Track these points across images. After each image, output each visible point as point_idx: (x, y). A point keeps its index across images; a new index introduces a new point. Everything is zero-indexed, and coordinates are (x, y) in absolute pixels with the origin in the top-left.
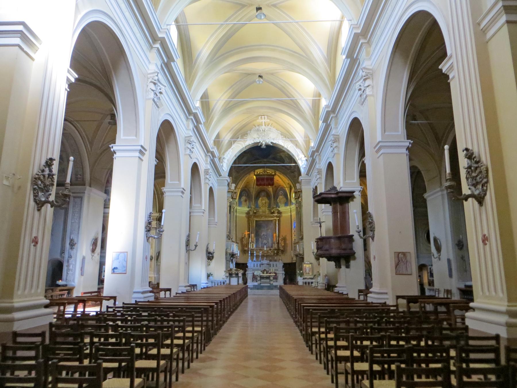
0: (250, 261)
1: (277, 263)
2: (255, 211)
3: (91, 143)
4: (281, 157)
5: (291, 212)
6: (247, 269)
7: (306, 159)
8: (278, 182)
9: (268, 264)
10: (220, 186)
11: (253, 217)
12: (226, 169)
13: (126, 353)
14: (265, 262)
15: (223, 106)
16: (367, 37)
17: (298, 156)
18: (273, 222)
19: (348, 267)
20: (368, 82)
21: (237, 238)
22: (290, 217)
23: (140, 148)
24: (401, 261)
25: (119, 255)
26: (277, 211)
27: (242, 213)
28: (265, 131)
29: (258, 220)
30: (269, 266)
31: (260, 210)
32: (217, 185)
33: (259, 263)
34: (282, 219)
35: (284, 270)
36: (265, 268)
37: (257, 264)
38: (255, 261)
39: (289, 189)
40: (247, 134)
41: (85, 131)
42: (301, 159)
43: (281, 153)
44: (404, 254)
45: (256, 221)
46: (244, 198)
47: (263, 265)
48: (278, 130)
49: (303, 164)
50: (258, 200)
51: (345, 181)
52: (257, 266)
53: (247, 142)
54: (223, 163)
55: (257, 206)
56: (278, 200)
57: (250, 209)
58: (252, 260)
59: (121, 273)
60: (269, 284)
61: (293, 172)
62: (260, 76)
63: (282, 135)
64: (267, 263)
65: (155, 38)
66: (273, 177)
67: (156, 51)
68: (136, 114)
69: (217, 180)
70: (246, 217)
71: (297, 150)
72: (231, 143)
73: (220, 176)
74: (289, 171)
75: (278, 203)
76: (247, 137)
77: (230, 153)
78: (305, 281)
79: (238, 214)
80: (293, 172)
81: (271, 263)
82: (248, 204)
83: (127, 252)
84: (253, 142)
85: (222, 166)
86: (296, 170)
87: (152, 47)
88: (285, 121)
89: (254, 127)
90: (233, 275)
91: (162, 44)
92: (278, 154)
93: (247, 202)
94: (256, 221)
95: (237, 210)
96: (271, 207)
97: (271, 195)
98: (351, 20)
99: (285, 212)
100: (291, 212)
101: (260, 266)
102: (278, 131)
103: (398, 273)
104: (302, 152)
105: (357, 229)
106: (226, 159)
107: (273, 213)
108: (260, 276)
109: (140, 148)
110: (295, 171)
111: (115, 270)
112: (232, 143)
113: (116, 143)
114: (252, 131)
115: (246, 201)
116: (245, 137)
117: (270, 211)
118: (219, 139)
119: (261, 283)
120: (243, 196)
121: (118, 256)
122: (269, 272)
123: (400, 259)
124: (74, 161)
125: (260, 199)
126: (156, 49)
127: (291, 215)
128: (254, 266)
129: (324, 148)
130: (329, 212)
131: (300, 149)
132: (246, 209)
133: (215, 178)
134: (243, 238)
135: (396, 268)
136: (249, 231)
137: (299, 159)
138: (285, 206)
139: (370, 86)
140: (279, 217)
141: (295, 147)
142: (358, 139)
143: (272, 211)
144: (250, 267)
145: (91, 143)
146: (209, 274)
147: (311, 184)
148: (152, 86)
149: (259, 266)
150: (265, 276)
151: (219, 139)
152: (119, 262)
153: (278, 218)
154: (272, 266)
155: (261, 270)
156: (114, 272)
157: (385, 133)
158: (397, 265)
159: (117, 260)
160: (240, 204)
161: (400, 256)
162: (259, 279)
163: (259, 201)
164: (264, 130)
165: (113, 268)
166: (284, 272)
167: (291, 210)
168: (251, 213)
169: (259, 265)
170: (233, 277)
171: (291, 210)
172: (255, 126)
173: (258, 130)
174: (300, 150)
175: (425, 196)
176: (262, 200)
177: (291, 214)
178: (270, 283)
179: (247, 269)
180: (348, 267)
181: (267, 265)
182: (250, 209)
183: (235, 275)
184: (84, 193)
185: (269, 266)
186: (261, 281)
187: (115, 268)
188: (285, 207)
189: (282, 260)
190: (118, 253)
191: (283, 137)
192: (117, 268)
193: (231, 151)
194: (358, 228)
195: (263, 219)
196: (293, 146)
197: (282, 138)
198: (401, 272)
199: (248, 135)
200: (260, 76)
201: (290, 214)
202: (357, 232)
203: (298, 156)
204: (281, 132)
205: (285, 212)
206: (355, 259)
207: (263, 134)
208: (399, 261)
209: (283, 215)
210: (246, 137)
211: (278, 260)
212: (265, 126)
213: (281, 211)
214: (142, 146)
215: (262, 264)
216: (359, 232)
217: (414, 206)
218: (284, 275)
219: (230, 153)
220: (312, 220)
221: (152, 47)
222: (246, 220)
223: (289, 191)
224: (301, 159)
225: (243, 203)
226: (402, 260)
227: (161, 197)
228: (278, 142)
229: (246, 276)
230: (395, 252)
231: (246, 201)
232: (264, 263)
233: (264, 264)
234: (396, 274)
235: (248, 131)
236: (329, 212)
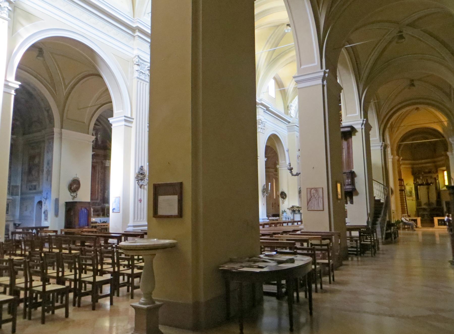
10: (290, 132)
12: (295, 115)
15: (266, 60)
19: (352, 202)
23: (124, 118)
24: (313, 197)
25: (116, 199)
44: (316, 190)
51: (346, 116)
54: (291, 110)
59: (117, 212)
65: (133, 29)
67: (138, 38)
68: (121, 93)
87: (134, 37)
90: (296, 212)
91: (140, 30)
103: (310, 209)
106: (293, 106)
109: (124, 118)
111: (114, 210)
113: (114, 116)
118: (284, 88)
121: (115, 200)
123: (312, 195)
126: (137, 36)
130: (373, 146)
142: (351, 71)
146: (283, 211)
148: (136, 68)
151: (281, 91)
156: (113, 211)
157: (301, 67)
165: (113, 209)
170: (296, 213)
180: (352, 202)
190: (115, 198)
198: (312, 209)
206: (357, 194)
208: (311, 197)
214: (125, 116)
221: (134, 37)
226: (314, 196)
236: (373, 146)
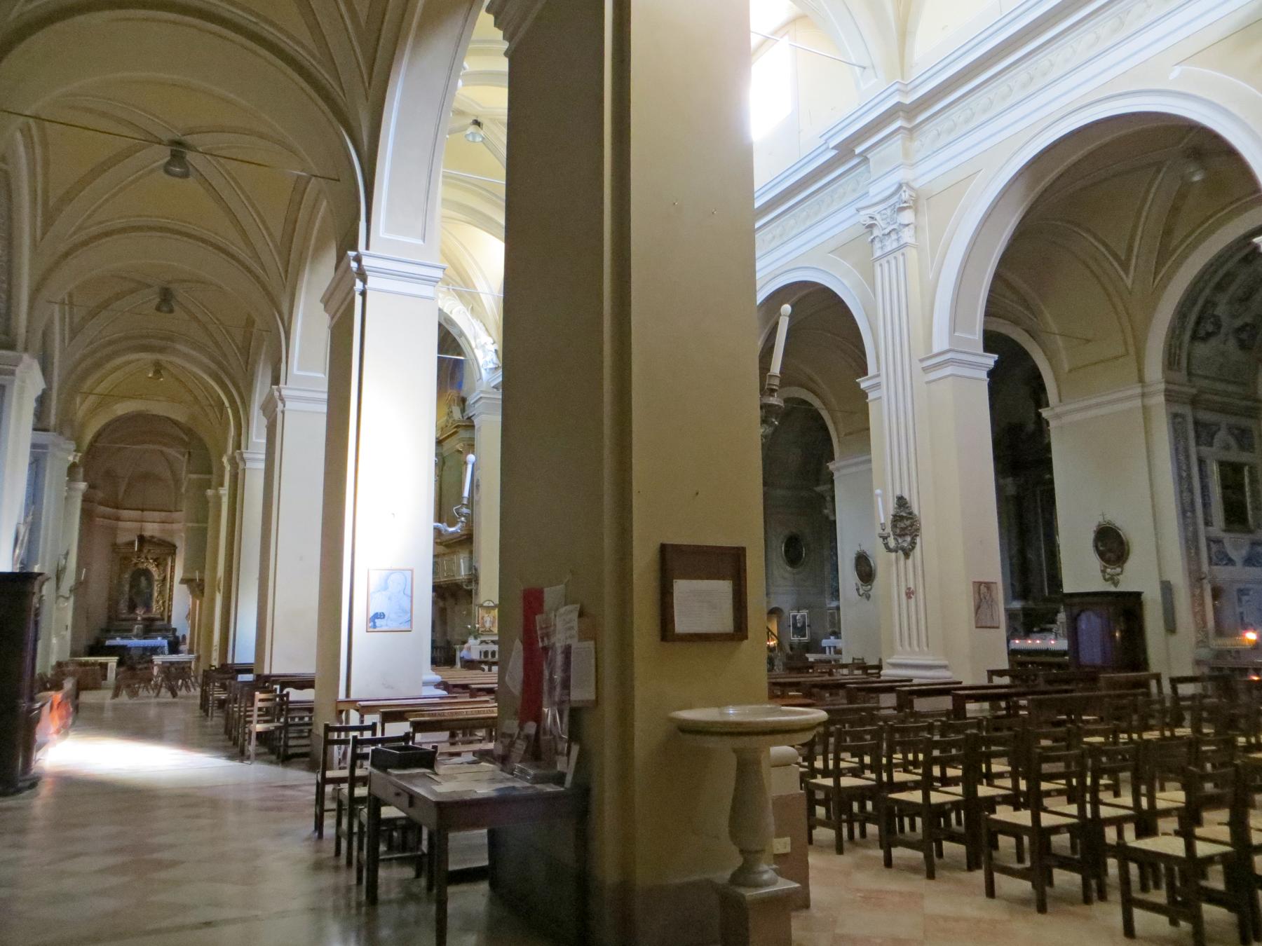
3: (49, 221)
7: (497, 348)
13: (942, 820)
16: (915, 116)
17: (475, 338)
20: (907, 217)
41: (238, 195)
42: (483, 346)
49: (488, 359)
62: (477, 123)
71: (474, 321)
78: (484, 647)
83: (412, 571)
88: (462, 244)
98: (864, 68)
104: (487, 330)
105: (881, 531)
111: (376, 620)
121: (386, 581)
124: (791, 317)
131: (481, 322)
135: (976, 613)
137: (476, 347)
139: (911, 226)
141: (469, 314)
145: (49, 221)
152: (390, 598)
156: (375, 626)
158: (978, 608)
159: (384, 593)
161: (982, 592)
165: (371, 614)
174: (481, 325)
175: (831, 466)
184: (12, 373)
187: (379, 616)
192: (384, 615)
194: (884, 530)
198: (984, 624)
200: (477, 123)
202: (881, 537)
203: (475, 338)
216: (885, 538)
217: (765, 484)
224: (483, 346)
227: (78, 405)
230: (974, 582)
234: (977, 627)
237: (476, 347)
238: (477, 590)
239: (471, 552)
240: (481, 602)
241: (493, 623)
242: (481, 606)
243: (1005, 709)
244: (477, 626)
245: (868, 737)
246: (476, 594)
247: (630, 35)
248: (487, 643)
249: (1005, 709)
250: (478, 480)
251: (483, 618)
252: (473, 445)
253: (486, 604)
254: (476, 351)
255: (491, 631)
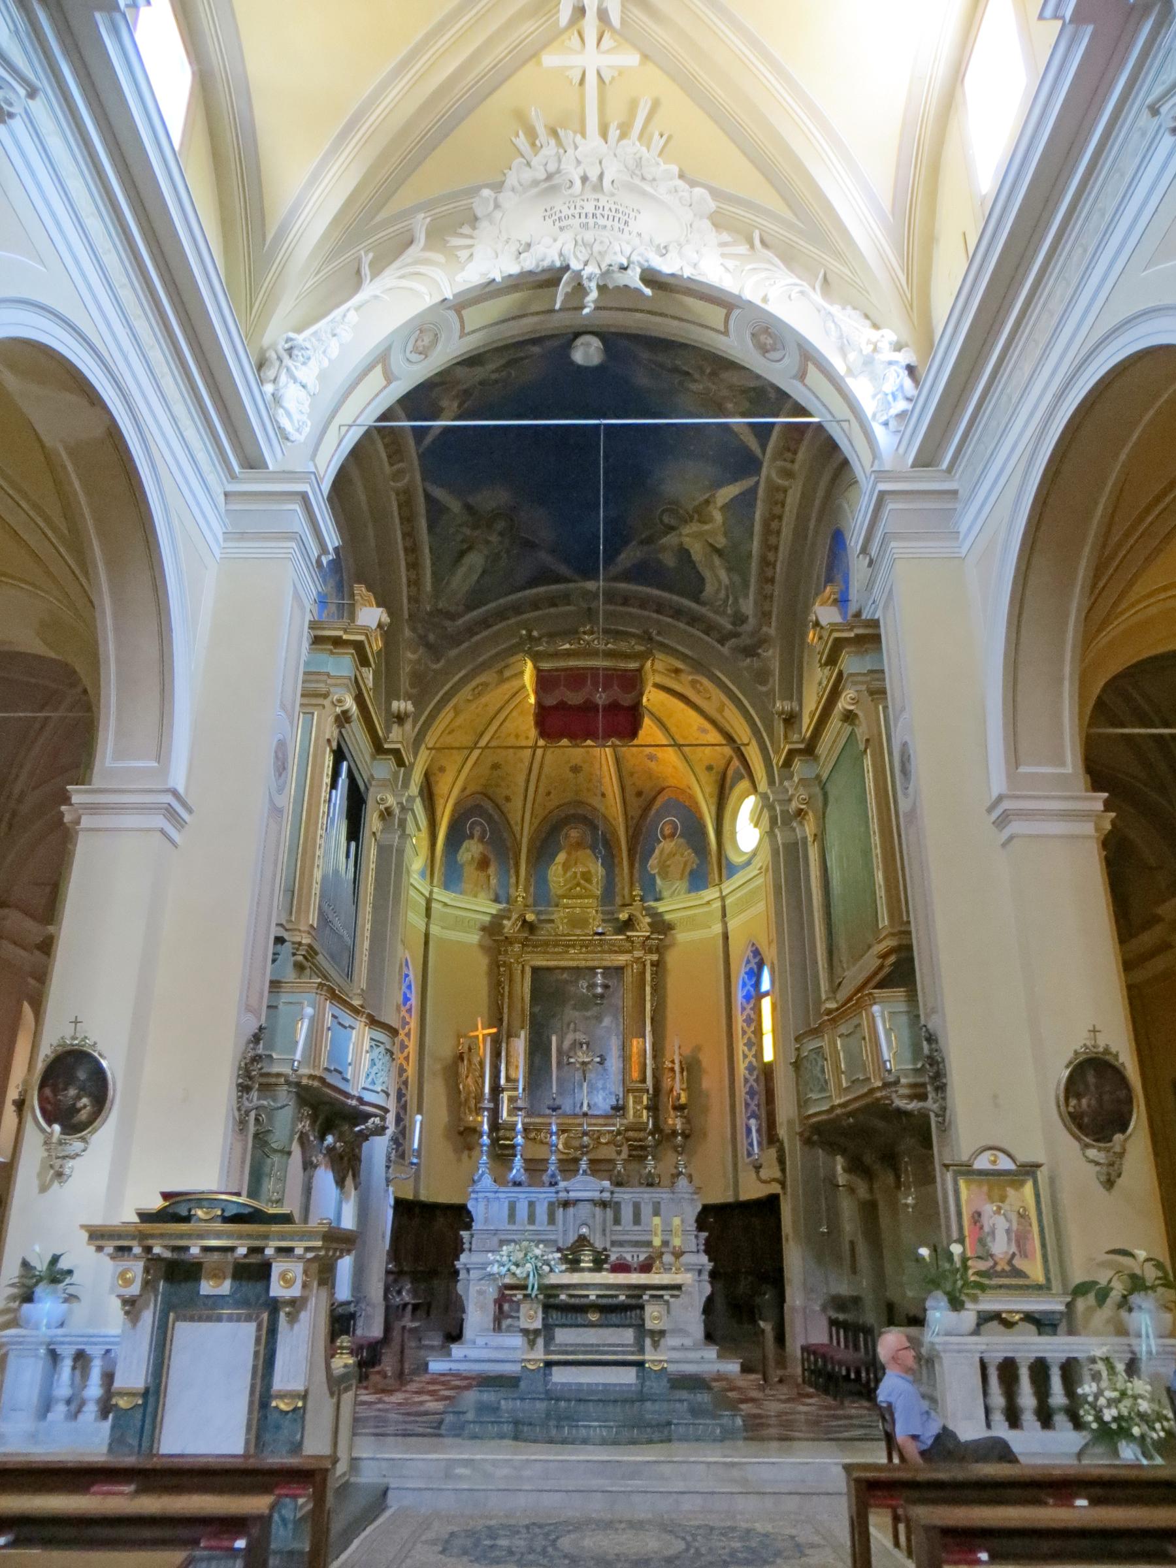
0: (487, 1181)
1: (661, 1194)
2: (530, 917)
4: (684, 554)
5: (724, 915)
6: (464, 1234)
8: (652, 765)
9: (604, 1204)
10: (242, 536)
11: (517, 947)
12: (306, 430)
14: (584, 1186)
18: (628, 977)
21: (427, 1061)
22: (720, 942)
26: (648, 920)
27: (459, 924)
28: (599, 187)
29: (544, 963)
30: (609, 1213)
31: (558, 915)
32: (219, 530)
33: (544, 1196)
34: (672, 959)
35: (707, 1242)
36: (584, 1230)
37: (531, 1204)
38: (517, 1184)
39: (711, 788)
40: (474, 220)
43: (687, 530)
45: (535, 970)
46: (471, 850)
47: (571, 1210)
48: (693, 184)
50: (548, 866)
52: (532, 1219)
53: (470, 267)
55: (542, 896)
56: (653, 861)
57: (502, 906)
58: (499, 1180)
60: (628, 1376)
61: (750, 651)
63: (718, 222)
64: (596, 1195)
66: (639, 670)
69: (226, 494)
70: (481, 946)
72: (358, 272)
73: (253, 462)
74: (725, 650)
75: (652, 878)
76: (471, 237)
77: (346, 335)
79: (435, 930)
80: (750, 651)
81: (625, 1196)
82: (493, 881)
84: (515, 269)
85: (277, 398)
86: (772, 631)
89: (522, 142)
92: (670, 540)
93: (492, 870)
94: (535, 970)
95: (434, 905)
96: (619, 901)
97: (618, 840)
99: (693, 923)
100: (724, 915)
101: (552, 1220)
102: (699, 191)
107: (629, 924)
108: (543, 1288)
110: (763, 641)
112: (366, 270)
114: (508, 199)
115: (483, 864)
116: (455, 241)
117: (609, 918)
119: (549, 1364)
120: (472, 837)
122: (613, 1258)
125: (561, 857)
127: (726, 937)
128: (512, 1216)
129: (989, 408)
132: (484, 907)
133: (212, 479)
134: (461, 1057)
136: (496, 1019)
137: (850, 371)
138: (690, 891)
140: (659, 949)
141: (817, 297)
143: (623, 916)
144: (486, 1220)
147: (963, 527)
149: (545, 1218)
150: (593, 1295)
153: (655, 957)
154: (627, 1213)
155: (555, 1241)
160: (452, 877)
162: (538, 1324)
163: (553, 868)
164: (593, 176)
166: (704, 1259)
167: (724, 908)
168: (509, 927)
169: (542, 1211)
170: (208, 1310)
171: (724, 908)
172: (532, 135)
173: (551, 184)
174: (856, 314)
176: (566, 866)
177: (725, 924)
178: (640, 1364)
179: (464, 1234)
181: (598, 1210)
182: (502, 906)
183: (226, 1287)
185: (609, 1213)
186: (549, 1340)
188: (693, 895)
189: (690, 1178)
191: (726, 237)
193: (353, 317)
195: (575, 959)
196: (807, 287)
197: (723, 244)
199: (484, 225)
201: (717, 928)
204: (715, 193)
205: (693, 923)
207: (589, 208)
209: (682, 936)
210: (468, 242)
211: (666, 1181)
212: (604, 134)
213: (667, 917)
215: (566, 1204)
218: (706, 1276)
219: (346, 335)
220: (998, 784)
222: (482, 962)
223: (713, 809)
225: (470, 872)
228: (695, 266)
229: (460, 1288)
231: (483, 864)
232: (573, 1195)
233: (577, 1201)
235: (474, 191)
237: (850, 371)
238: (943, 1112)
239: (912, 997)
240: (965, 1158)
241: (1020, 1239)
242: (966, 1170)
243: (1079, 1100)
244: (956, 1249)
245: (636, 1044)
246: (944, 1127)
247: (1015, 577)
248: (1008, 1324)
249: (1079, 1100)
250: (905, 745)
251: (977, 1216)
252: (883, 692)
253: (982, 1163)
254: (850, 381)
255: (1018, 1273)
